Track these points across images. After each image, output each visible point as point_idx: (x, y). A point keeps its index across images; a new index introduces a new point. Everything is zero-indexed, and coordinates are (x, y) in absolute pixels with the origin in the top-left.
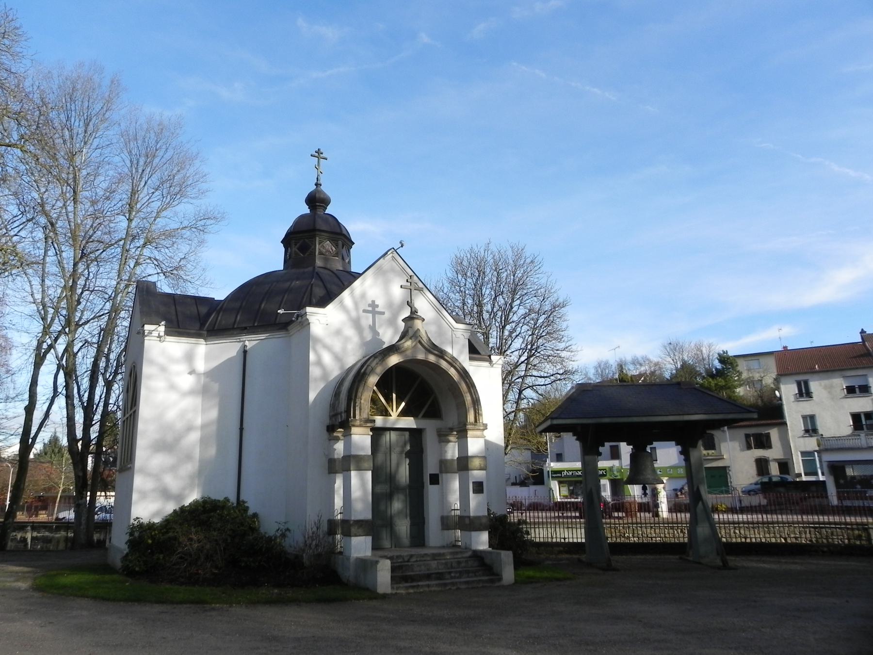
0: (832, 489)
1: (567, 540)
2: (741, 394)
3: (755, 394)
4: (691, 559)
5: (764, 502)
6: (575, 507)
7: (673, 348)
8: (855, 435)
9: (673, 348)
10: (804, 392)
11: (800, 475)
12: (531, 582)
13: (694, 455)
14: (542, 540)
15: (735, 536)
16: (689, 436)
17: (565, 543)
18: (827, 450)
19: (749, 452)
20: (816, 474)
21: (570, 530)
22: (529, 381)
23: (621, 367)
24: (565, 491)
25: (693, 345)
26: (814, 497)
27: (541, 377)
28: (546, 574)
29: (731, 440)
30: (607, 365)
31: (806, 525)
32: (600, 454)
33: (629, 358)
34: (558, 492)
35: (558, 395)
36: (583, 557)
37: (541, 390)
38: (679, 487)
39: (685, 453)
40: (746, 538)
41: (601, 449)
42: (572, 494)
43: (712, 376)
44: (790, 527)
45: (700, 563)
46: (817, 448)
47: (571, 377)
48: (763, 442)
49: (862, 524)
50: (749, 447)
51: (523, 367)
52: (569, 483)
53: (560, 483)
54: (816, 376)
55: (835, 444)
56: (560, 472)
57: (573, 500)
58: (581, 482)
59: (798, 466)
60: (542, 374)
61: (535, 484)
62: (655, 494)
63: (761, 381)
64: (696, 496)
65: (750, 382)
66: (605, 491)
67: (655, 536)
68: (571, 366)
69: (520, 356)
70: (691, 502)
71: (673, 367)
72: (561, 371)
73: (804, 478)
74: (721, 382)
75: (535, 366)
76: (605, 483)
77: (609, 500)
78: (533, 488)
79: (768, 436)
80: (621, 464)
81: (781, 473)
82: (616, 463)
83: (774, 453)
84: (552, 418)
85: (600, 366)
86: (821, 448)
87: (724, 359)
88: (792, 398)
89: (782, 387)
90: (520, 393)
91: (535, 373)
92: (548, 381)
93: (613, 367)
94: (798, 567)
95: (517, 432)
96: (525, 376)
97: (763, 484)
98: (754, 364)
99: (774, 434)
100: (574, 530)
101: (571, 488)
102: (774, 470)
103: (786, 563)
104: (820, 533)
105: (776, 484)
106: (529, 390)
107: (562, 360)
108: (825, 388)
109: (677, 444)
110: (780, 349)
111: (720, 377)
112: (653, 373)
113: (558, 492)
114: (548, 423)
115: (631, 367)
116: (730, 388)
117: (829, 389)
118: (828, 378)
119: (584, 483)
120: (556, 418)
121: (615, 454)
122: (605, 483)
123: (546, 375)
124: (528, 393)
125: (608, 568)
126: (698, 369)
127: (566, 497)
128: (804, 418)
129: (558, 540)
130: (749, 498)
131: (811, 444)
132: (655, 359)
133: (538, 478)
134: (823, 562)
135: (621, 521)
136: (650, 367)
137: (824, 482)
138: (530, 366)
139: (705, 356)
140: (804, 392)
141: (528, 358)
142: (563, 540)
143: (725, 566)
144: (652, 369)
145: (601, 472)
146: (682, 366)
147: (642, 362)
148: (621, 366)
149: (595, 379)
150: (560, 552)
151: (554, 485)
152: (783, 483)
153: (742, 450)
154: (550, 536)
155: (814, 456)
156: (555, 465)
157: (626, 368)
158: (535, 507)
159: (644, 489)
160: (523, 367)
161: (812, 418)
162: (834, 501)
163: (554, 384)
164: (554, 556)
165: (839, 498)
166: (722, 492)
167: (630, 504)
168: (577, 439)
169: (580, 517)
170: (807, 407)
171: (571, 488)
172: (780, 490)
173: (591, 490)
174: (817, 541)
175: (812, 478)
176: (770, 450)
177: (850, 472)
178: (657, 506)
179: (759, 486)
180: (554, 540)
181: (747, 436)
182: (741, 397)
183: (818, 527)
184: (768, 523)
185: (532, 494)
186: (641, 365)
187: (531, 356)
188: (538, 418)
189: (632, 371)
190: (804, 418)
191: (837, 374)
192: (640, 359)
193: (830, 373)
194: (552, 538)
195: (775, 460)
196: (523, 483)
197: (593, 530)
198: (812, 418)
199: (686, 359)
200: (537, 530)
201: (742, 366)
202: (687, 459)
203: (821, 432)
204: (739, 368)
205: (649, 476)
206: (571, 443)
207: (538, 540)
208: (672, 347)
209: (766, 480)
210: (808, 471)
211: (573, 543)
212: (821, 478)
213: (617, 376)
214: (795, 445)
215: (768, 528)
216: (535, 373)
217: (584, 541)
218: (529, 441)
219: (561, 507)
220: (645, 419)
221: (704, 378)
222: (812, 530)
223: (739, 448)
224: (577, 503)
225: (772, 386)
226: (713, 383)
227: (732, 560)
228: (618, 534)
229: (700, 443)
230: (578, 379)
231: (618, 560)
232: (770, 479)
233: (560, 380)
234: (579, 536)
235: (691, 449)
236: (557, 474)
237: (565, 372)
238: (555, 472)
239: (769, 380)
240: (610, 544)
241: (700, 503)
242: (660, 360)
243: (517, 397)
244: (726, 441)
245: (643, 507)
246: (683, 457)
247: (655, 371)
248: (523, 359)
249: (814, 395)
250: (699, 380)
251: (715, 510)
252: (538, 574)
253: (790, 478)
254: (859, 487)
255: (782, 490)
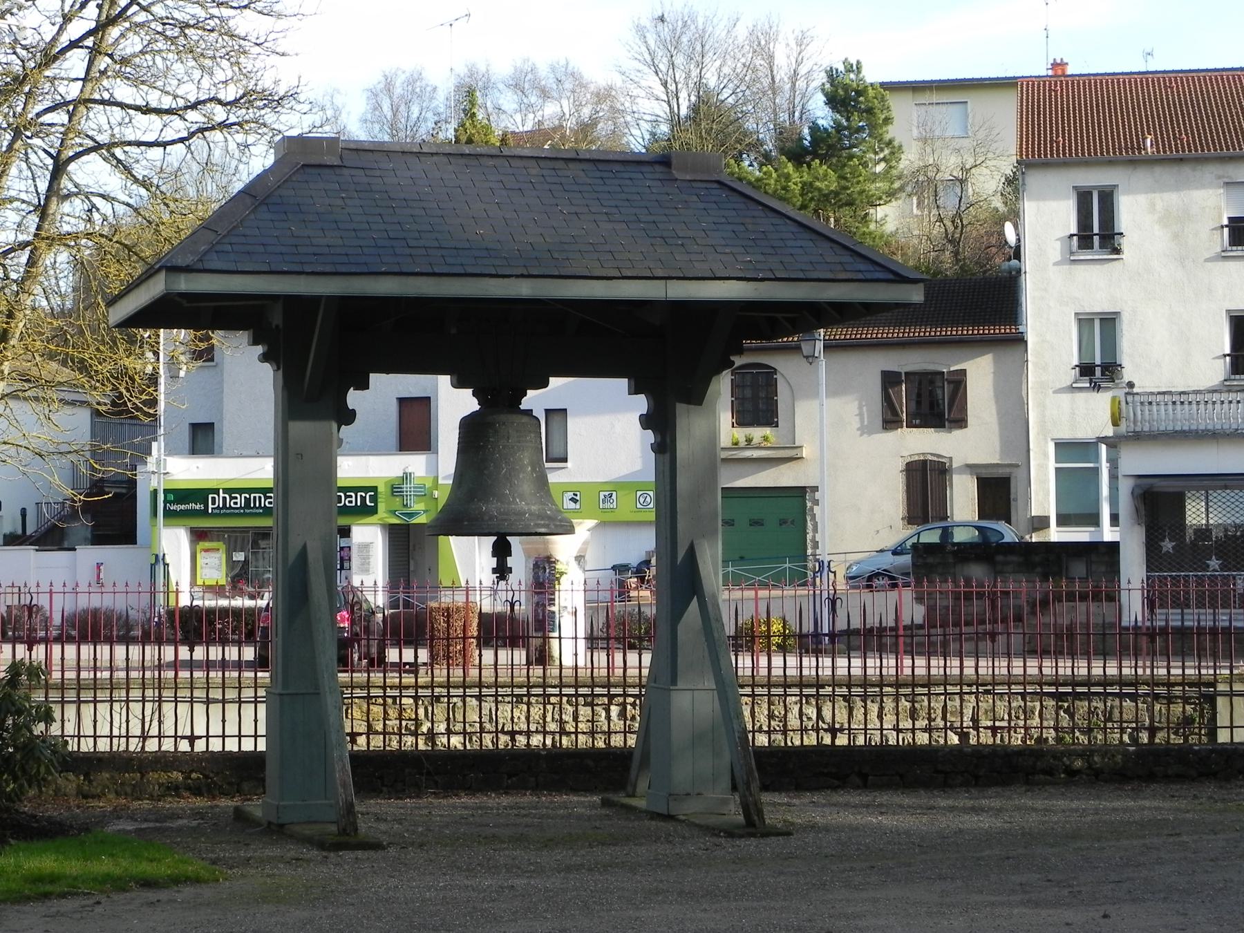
0: (1133, 568)
1: (200, 746)
2: (890, 227)
3: (937, 230)
4: (640, 803)
5: (915, 613)
6: (244, 626)
7: (674, 40)
8: (1230, 390)
9: (674, 40)
10: (1097, 232)
11: (1041, 523)
12: (46, 896)
13: (690, 427)
14: (103, 745)
15: (802, 726)
16: (670, 355)
17: (191, 756)
18: (1137, 437)
19: (892, 437)
20: (1093, 519)
21: (215, 709)
22: (98, 122)
23: (468, 96)
24: (214, 568)
25: (741, 33)
26: (1071, 597)
27: (146, 110)
28: (104, 866)
29: (832, 393)
30: (416, 88)
31: (1038, 688)
32: (348, 417)
33: (502, 68)
34: (186, 568)
35: (210, 187)
36: (256, 807)
37: (147, 162)
38: (634, 560)
39: (659, 422)
40: (833, 731)
41: (354, 398)
42: (240, 578)
43: (798, 155)
44: (990, 694)
45: (669, 817)
46: (1109, 431)
47: (269, 117)
48: (936, 403)
49: (1198, 683)
50: (890, 421)
51: (76, 63)
52: (233, 539)
53: (198, 535)
54: (1141, 176)
55: (1164, 418)
56: (200, 495)
57: (238, 602)
58: (264, 534)
59: (1042, 494)
60: (154, 99)
61: (99, 539)
62: (544, 577)
63: (962, 182)
64: (680, 579)
65: (925, 186)
66: (366, 569)
67: (529, 726)
68: (272, 74)
69: (67, 19)
70: (667, 604)
71: (662, 110)
72: (230, 94)
73: (1055, 534)
74: (825, 177)
75: (124, 61)
76: (369, 538)
77: (379, 599)
78: (88, 556)
79: (958, 382)
80: (434, 468)
81: (982, 516)
82: (416, 464)
83: (968, 446)
84: (173, 269)
85: (389, 87)
86: (1123, 428)
87: (846, 95)
88: (1055, 251)
89: (1030, 208)
90: (59, 168)
91: (124, 92)
92: (177, 128)
93: (441, 96)
94: (984, 822)
95: (34, 329)
96: (85, 102)
97: (921, 551)
98: (946, 118)
99: (980, 373)
100: (232, 710)
101: (239, 556)
102: (963, 502)
103: (952, 809)
104: (1071, 713)
105: (966, 553)
106: (94, 162)
107: (237, 47)
108: (1166, 219)
109: (635, 390)
110: (1040, 69)
111: (824, 159)
112: (586, 128)
113: (186, 568)
114: (156, 288)
115: (508, 101)
116: (852, 201)
117: (1176, 222)
118: (1177, 188)
119: (285, 538)
120: (188, 270)
121: (414, 429)
122: (369, 538)
123: (167, 102)
124: (90, 172)
125: (346, 839)
126: (750, 125)
127: (217, 590)
128: (1084, 321)
129: (168, 745)
130: (867, 596)
131: (1092, 415)
132: (598, 75)
133: (109, 514)
134: (1061, 803)
135: (408, 679)
136: (578, 106)
137: (1114, 547)
138: (103, 62)
139: (782, 74)
140: (1097, 232)
141: (101, 28)
142: (184, 746)
143: (753, 825)
144: (586, 112)
145: (354, 500)
146: (695, 109)
147: (550, 83)
148: (470, 93)
149: (356, 124)
150: (173, 789)
151: (174, 543)
152: (987, 551)
153: (865, 430)
154: (136, 730)
155: (1097, 458)
156: (187, 470)
157: (485, 104)
158: (90, 628)
159: (501, 551)
160: (76, 63)
161: (1109, 322)
162: (1133, 607)
163: (196, 142)
164: (146, 804)
165: (1151, 603)
166: (778, 580)
167: (448, 613)
168: (265, 358)
169: (261, 663)
170: (1096, 284)
171: (239, 556)
172: (978, 572)
173: (303, 553)
174: (1059, 740)
175: (1080, 535)
176: (957, 433)
177: (1196, 514)
178: (544, 622)
179: (906, 559)
180: (152, 746)
181: (890, 380)
182: (887, 240)
183: (1067, 693)
184: (913, 683)
185: (85, 575)
186: (545, 94)
187: (112, 21)
188: (118, 273)
189: (510, 116)
190: (1084, 321)
191: (1211, 172)
192: (543, 71)
193: (1186, 170)
194: (144, 737)
195: (971, 468)
196: (51, 537)
197: (300, 706)
198: (1109, 322)
199: (711, 80)
200: (87, 710)
201: (904, 123)
202: (664, 447)
203: (1128, 374)
204: (891, 132)
205: (523, 501)
206: (246, 378)
207: (87, 746)
208: (665, 31)
209: (931, 537)
210: (1071, 509)
211: (225, 756)
212: (1108, 534)
213: (449, 132)
214: (1036, 418)
215: (913, 698)
216: (124, 92)
217: (262, 746)
218: (83, 367)
219: (193, 626)
220: (525, 289)
221: (767, 158)
222: (1050, 703)
223: (856, 423)
224: (251, 612)
225: (997, 203)
226: (796, 177)
227: (780, 808)
228: (393, 723)
229: (723, 387)
230: (294, 123)
231: (380, 813)
232: (946, 533)
233: (223, 126)
234: (248, 729)
235: (681, 408)
236: (186, 503)
237: (246, 99)
238: (181, 495)
239: (987, 185)
240: (356, 758)
241: (694, 603)
242: (618, 81)
243: (43, 186)
244: (816, 395)
245: (498, 630)
246: (650, 436)
247: (593, 122)
248: (76, 29)
249: (1125, 244)
250: (750, 167)
251: (747, 639)
252: (73, 866)
253: (1009, 534)
254: (1214, 563)
255: (977, 571)
